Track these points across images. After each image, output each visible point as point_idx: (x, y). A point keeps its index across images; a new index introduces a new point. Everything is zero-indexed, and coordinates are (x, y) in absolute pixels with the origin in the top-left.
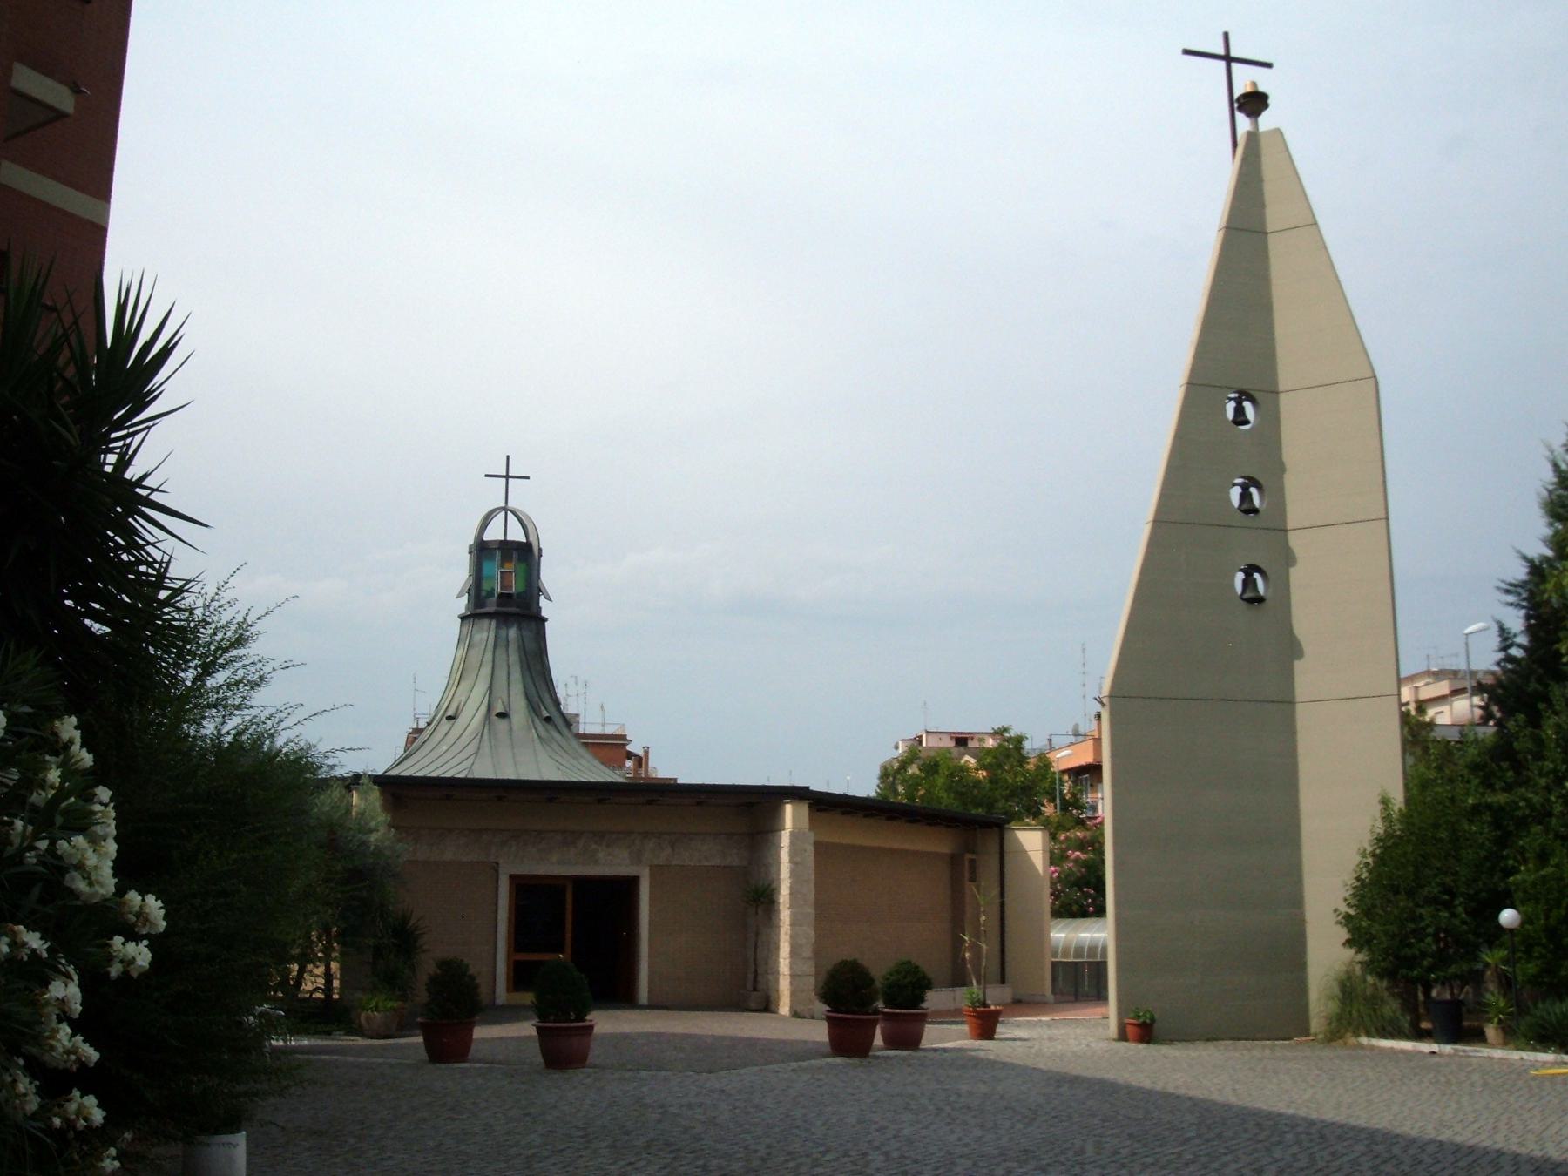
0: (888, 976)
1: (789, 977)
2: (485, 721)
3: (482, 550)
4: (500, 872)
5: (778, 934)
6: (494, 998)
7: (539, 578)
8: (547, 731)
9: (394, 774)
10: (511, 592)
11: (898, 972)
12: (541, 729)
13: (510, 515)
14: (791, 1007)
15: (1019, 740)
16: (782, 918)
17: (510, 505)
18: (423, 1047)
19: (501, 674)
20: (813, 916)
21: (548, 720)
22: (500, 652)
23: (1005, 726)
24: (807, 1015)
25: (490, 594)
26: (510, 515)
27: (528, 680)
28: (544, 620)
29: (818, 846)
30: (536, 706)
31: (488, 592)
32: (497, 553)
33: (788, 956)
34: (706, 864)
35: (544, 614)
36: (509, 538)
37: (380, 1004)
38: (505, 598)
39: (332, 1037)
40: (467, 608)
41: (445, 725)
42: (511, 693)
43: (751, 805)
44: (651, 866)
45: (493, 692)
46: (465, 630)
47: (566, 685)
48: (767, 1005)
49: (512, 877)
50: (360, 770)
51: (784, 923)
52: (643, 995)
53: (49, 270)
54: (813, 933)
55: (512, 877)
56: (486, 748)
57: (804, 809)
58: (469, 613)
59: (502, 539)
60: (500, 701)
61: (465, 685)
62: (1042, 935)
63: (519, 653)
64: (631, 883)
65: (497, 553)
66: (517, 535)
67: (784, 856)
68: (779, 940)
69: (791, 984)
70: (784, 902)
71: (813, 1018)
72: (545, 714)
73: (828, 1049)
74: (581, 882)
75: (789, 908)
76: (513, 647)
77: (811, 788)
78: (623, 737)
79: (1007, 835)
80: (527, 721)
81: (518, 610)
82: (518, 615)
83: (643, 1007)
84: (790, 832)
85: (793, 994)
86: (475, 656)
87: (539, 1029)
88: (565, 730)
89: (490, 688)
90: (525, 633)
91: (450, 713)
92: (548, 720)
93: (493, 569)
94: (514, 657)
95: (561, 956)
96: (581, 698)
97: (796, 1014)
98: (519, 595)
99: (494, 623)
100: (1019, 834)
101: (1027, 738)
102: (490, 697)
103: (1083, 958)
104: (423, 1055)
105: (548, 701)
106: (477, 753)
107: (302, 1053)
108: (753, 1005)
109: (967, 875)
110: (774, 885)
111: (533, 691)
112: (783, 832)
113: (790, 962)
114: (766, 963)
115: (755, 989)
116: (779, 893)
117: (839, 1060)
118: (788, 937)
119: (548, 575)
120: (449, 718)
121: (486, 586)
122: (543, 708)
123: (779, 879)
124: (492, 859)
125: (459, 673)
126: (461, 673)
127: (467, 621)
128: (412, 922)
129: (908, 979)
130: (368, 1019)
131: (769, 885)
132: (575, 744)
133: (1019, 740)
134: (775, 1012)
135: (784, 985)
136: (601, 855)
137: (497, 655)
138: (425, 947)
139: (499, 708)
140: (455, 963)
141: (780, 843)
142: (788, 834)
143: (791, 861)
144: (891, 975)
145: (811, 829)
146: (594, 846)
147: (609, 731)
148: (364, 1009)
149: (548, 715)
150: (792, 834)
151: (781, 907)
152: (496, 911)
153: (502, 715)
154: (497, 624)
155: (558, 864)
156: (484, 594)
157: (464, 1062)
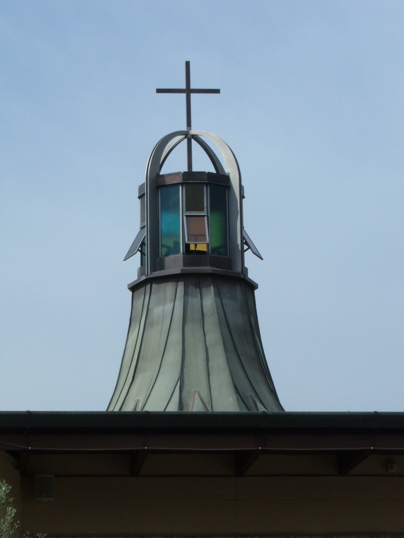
27: (241, 373)
35: (252, 276)
40: (141, 272)
42: (213, 385)
60: (197, 396)
89: (181, 379)
90: (226, 301)
127: (137, 293)
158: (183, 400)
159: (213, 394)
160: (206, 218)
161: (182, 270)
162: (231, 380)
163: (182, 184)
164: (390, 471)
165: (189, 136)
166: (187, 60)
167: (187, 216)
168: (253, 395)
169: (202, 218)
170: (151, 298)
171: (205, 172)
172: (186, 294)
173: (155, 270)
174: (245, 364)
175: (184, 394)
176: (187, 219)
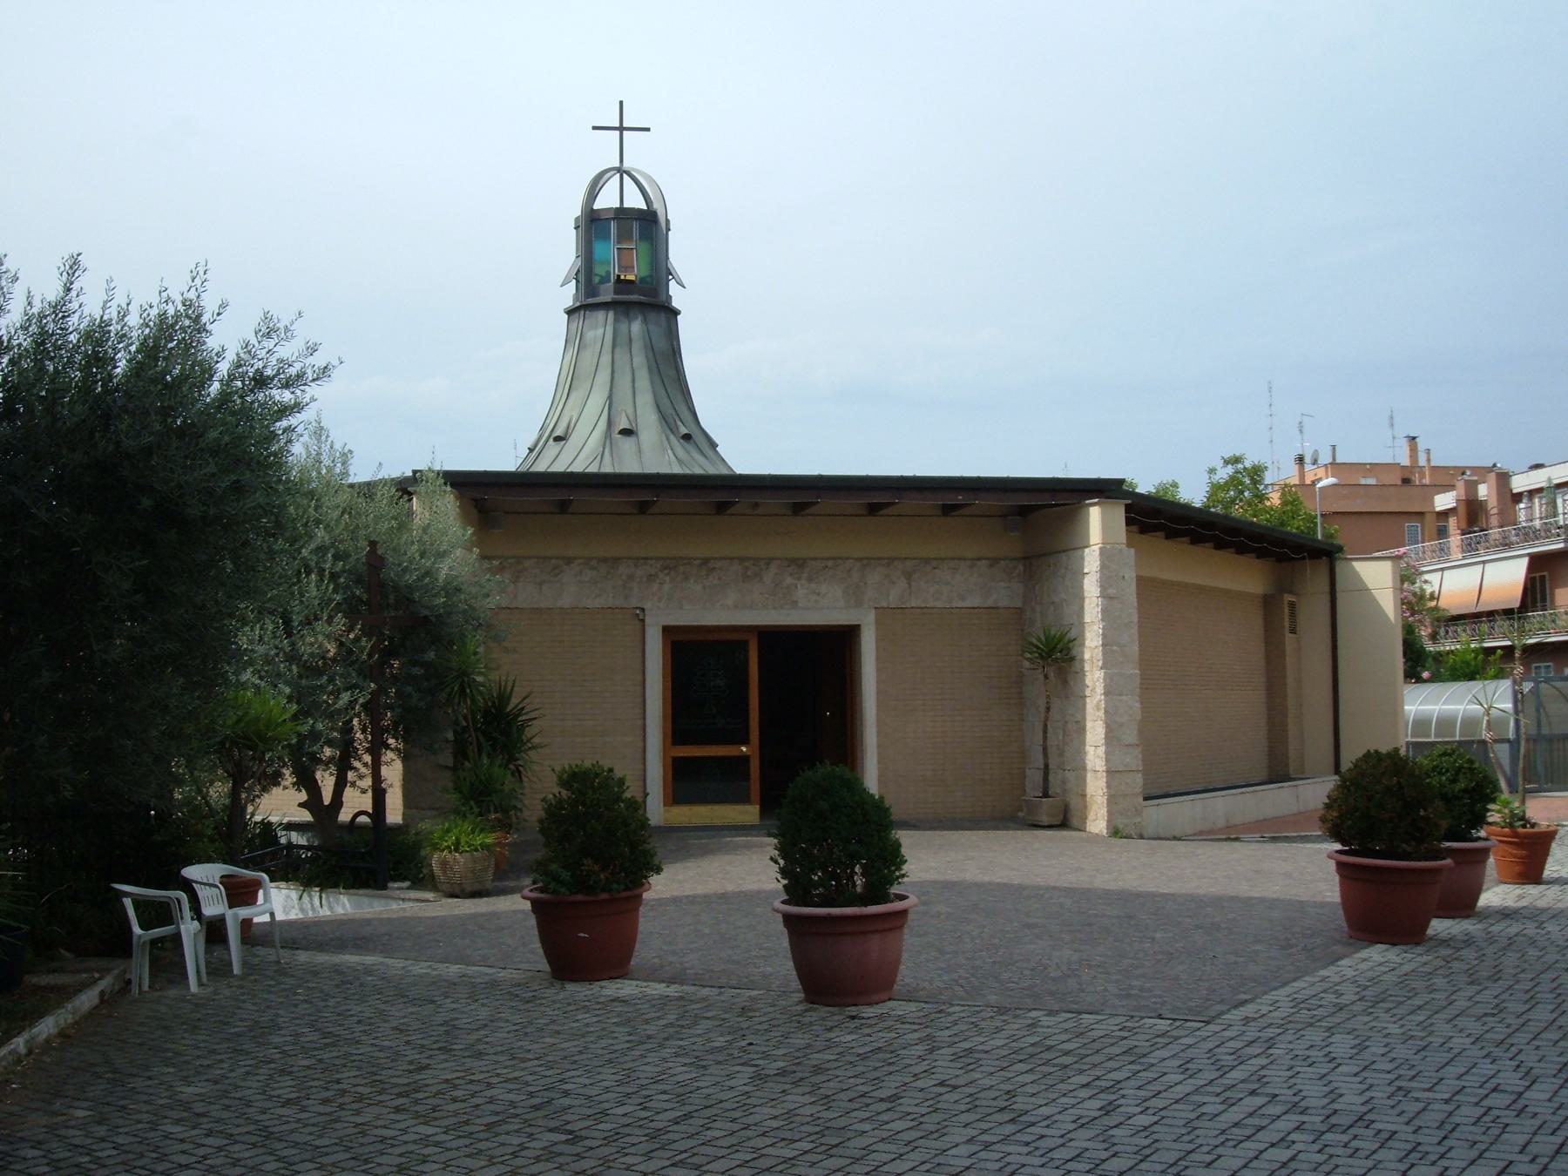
1: (1105, 774)
3: (593, 224)
4: (648, 621)
7: (667, 258)
14: (1109, 821)
15: (1256, 472)
16: (1088, 681)
17: (626, 165)
19: (624, 381)
21: (687, 437)
23: (1237, 455)
24: (1133, 833)
25: (605, 279)
30: (671, 421)
32: (613, 224)
35: (675, 304)
37: (463, 840)
40: (576, 298)
41: (553, 448)
43: (1024, 511)
45: (614, 405)
46: (574, 326)
48: (1065, 820)
49: (667, 631)
50: (422, 466)
51: (1093, 689)
53: (513, 687)
54: (1138, 705)
55: (667, 631)
57: (1119, 513)
58: (578, 304)
62: (1395, 705)
64: (843, 640)
65: (613, 224)
66: (635, 201)
67: (1091, 587)
68: (1084, 718)
69: (1109, 785)
71: (1141, 837)
72: (684, 430)
74: (772, 638)
76: (637, 346)
79: (1340, 567)
80: (662, 441)
82: (640, 304)
84: (1100, 548)
85: (1112, 800)
86: (589, 358)
88: (709, 452)
89: (610, 398)
90: (652, 327)
91: (558, 432)
92: (687, 437)
93: (608, 252)
94: (639, 359)
95: (744, 749)
97: (1115, 832)
98: (643, 280)
99: (611, 315)
100: (1358, 566)
101: (1266, 467)
102: (609, 408)
103: (1429, 736)
104: (534, 956)
105: (686, 414)
107: (321, 946)
108: (1045, 820)
109: (1287, 624)
110: (1073, 634)
111: (665, 402)
112: (1087, 550)
114: (1061, 754)
115: (1046, 795)
116: (1083, 644)
118: (1101, 713)
119: (680, 252)
120: (558, 439)
121: (599, 270)
122: (679, 423)
123: (1082, 624)
124: (634, 602)
126: (570, 382)
128: (514, 701)
129: (1462, 784)
130: (444, 864)
133: (1256, 472)
134: (1082, 829)
135: (1096, 787)
136: (801, 593)
137: (617, 356)
138: (536, 740)
139: (623, 424)
140: (597, 775)
141: (1082, 567)
142: (1097, 553)
143: (1104, 594)
145: (1130, 544)
146: (789, 580)
148: (435, 847)
149: (686, 431)
150: (1103, 552)
151: (1087, 667)
153: (627, 432)
155: (736, 607)
156: (597, 280)
157: (624, 976)
163: (614, 219)
172: (616, 320)
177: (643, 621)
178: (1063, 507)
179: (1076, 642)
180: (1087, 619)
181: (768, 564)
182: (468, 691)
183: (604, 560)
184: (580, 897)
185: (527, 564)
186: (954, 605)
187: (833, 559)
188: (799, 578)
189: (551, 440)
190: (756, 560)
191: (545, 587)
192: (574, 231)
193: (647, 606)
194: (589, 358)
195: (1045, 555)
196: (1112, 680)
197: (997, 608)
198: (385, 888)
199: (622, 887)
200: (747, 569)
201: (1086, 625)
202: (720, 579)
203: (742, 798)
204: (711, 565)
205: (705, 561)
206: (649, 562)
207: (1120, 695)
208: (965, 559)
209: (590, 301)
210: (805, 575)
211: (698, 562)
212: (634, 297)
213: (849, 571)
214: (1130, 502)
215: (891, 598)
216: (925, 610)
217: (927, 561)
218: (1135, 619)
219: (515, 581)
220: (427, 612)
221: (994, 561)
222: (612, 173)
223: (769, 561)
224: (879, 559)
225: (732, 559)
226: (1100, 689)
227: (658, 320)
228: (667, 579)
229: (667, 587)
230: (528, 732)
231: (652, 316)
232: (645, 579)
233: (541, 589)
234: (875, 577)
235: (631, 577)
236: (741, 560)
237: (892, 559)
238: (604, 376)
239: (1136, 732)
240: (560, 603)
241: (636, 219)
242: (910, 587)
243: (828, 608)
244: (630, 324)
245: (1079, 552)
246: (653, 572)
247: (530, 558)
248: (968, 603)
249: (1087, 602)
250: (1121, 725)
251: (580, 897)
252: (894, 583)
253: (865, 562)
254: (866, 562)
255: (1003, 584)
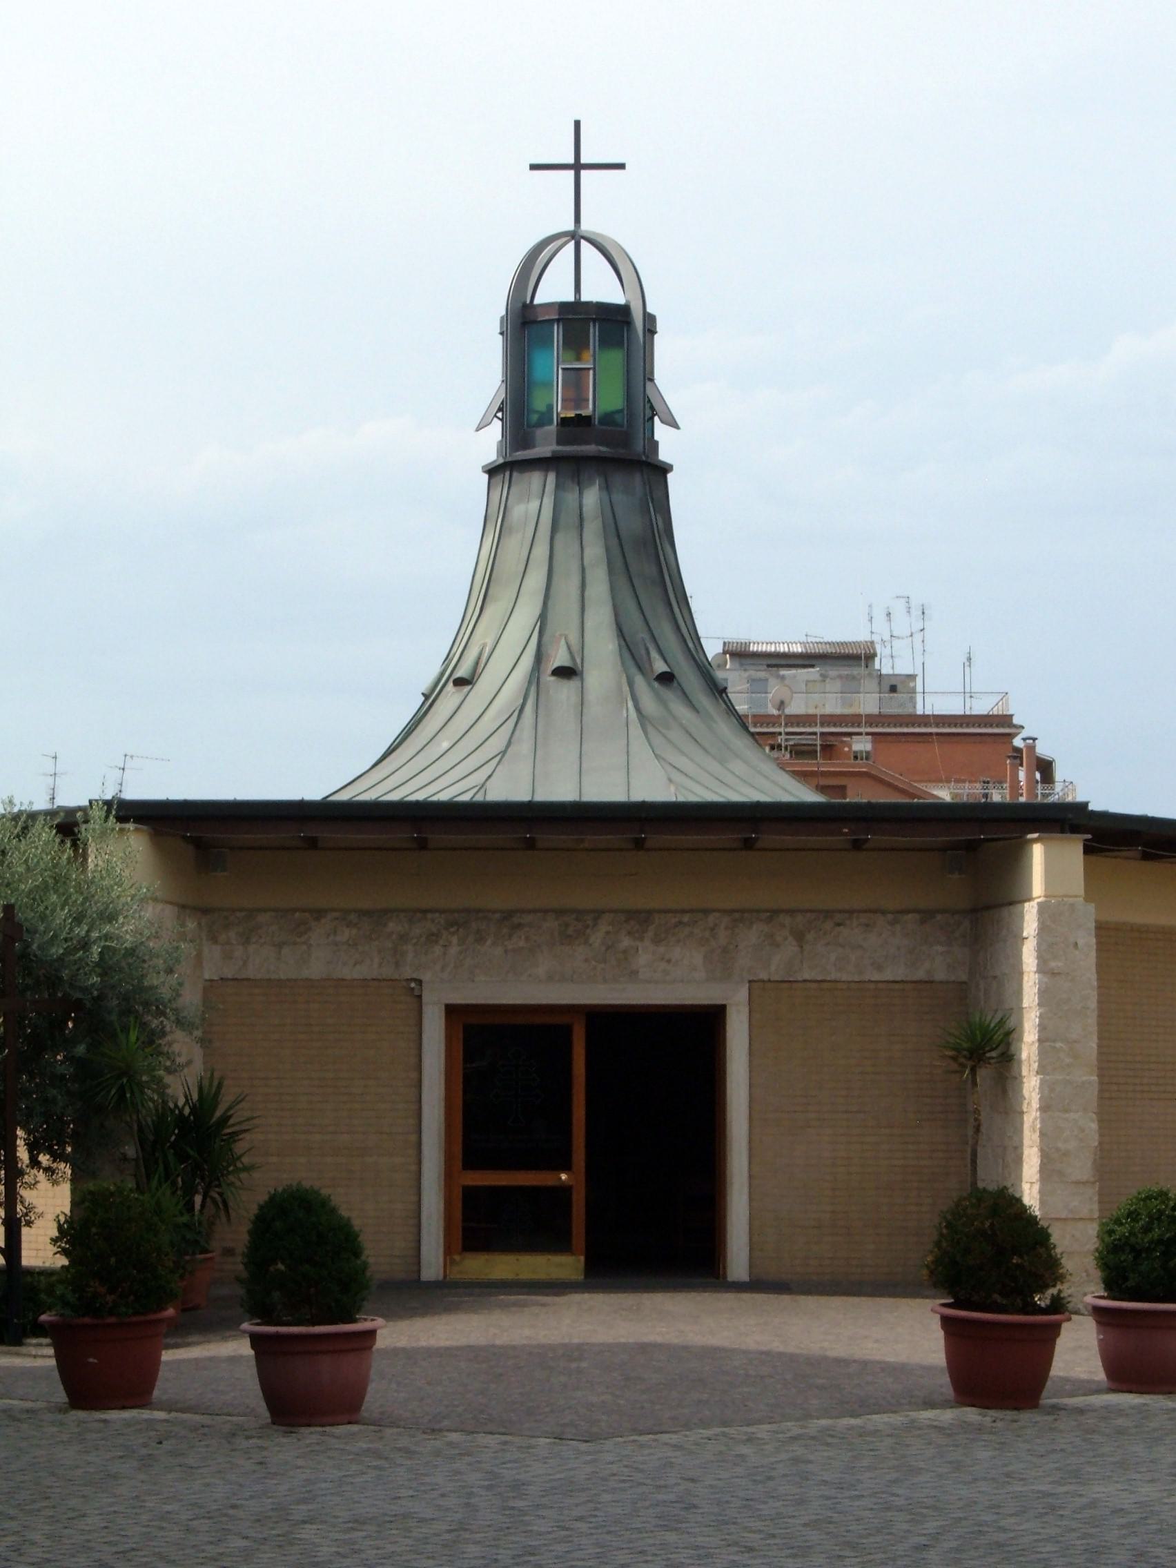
0: (1111, 1226)
2: (530, 683)
4: (425, 999)
5: (1020, 1131)
6: (419, 1271)
8: (663, 703)
9: (373, 797)
10: (584, 413)
11: (1133, 1215)
12: (649, 704)
13: (586, 248)
16: (1026, 1092)
17: (586, 226)
18: (56, 1374)
19: (568, 587)
20: (1093, 1093)
21: (666, 679)
22: (566, 542)
26: (583, 242)
27: (631, 605)
28: (663, 470)
29: (1102, 929)
31: (542, 414)
33: (1037, 1176)
34: (876, 976)
35: (664, 455)
36: (586, 297)
38: (575, 427)
39: (23, 1350)
40: (502, 447)
41: (451, 697)
42: (589, 624)
43: (971, 846)
44: (750, 982)
47: (889, 614)
49: (452, 1011)
52: (738, 1262)
54: (1094, 1126)
55: (452, 1011)
56: (524, 746)
57: (1072, 851)
59: (569, 297)
60: (563, 642)
61: (495, 611)
63: (606, 539)
70: (1029, 1057)
72: (660, 667)
73: (948, 1391)
75: (1038, 1073)
76: (593, 529)
77: (1091, 807)
78: (1006, 720)
81: (603, 449)
83: (739, 1287)
86: (515, 548)
87: (257, 1341)
89: (543, 618)
90: (618, 497)
92: (666, 679)
94: (595, 550)
95: (564, 1177)
96: (918, 638)
98: (608, 419)
99: (551, 478)
106: (504, 753)
110: (1011, 1023)
112: (1026, 905)
113: (1040, 1192)
116: (1020, 1039)
117: (971, 1414)
118: (1036, 1136)
120: (460, 682)
121: (539, 403)
122: (654, 654)
124: (408, 972)
125: (483, 591)
127: (499, 478)
129: (1156, 1233)
131: (1002, 1022)
132: (725, 728)
138: (245, 1160)
139: (560, 658)
141: (1022, 929)
143: (1042, 969)
144: (1118, 1222)
145: (1088, 897)
146: (626, 942)
147: (981, 707)
151: (1024, 1072)
152: (419, 1084)
153: (565, 673)
154: (557, 477)
158: (543, 649)
159: (586, 639)
160: (591, 372)
161: (553, 452)
162: (613, 618)
163: (558, 321)
164: (582, 846)
165: (577, 237)
166: (578, 118)
167: (563, 369)
168: (647, 637)
169: (586, 371)
170: (511, 492)
171: (591, 302)
172: (558, 487)
173: (517, 450)
174: (640, 591)
175: (546, 638)
176: (563, 374)
177: (420, 997)
178: (1001, 843)
179: (1014, 1035)
180: (1025, 1004)
181: (596, 920)
182: (128, 1095)
183: (363, 913)
184: (87, 1320)
185: (262, 918)
186: (867, 978)
187: (691, 911)
188: (641, 939)
189: (450, 684)
190: (579, 913)
191: (286, 951)
192: (501, 337)
193: (426, 977)
194: (515, 548)
195: (988, 908)
196: (1052, 1090)
197: (932, 982)
198: (19, 1343)
199: (131, 1311)
200: (567, 925)
201: (1024, 1011)
202: (527, 939)
203: (557, 1241)
204: (516, 920)
205: (508, 915)
206: (429, 916)
207: (1066, 1111)
208: (884, 913)
209: (521, 455)
210: (650, 934)
211: (497, 916)
212: (591, 449)
213: (712, 929)
214: (1089, 836)
215: (773, 968)
216: (825, 985)
217: (828, 914)
218: (1093, 1004)
219: (246, 941)
220: (78, 995)
221: (926, 915)
222: (565, 239)
223: (598, 914)
224: (758, 911)
225: (546, 911)
226: (1035, 1104)
227: (630, 488)
228: (455, 940)
229: (454, 950)
230: (239, 1148)
231: (618, 479)
232: (423, 939)
233: (280, 952)
234: (752, 935)
235: (404, 938)
236: (560, 912)
237: (775, 913)
238: (536, 580)
239: (1089, 1164)
240: (305, 973)
241: (594, 320)
242: (802, 952)
243: (682, 981)
244: (581, 493)
245: (1019, 906)
246: (434, 930)
247: (265, 910)
248: (888, 975)
249: (1025, 978)
250: (1066, 1154)
251: (87, 1320)
252: (778, 946)
253: (737, 915)
254: (740, 916)
255: (940, 948)
